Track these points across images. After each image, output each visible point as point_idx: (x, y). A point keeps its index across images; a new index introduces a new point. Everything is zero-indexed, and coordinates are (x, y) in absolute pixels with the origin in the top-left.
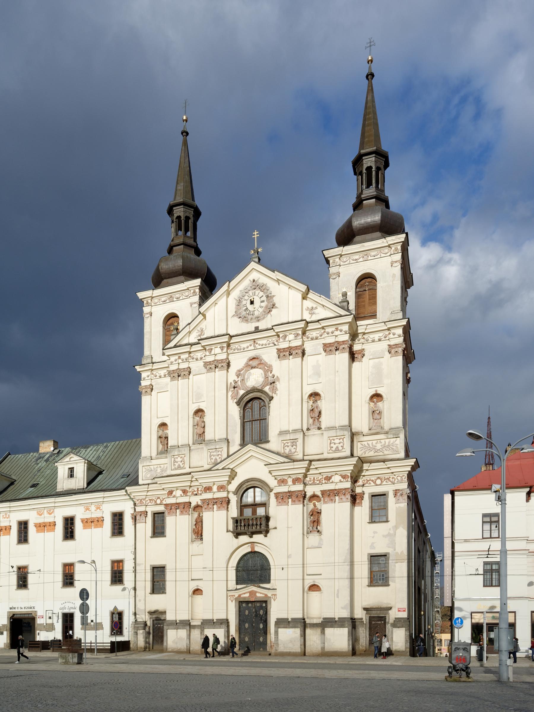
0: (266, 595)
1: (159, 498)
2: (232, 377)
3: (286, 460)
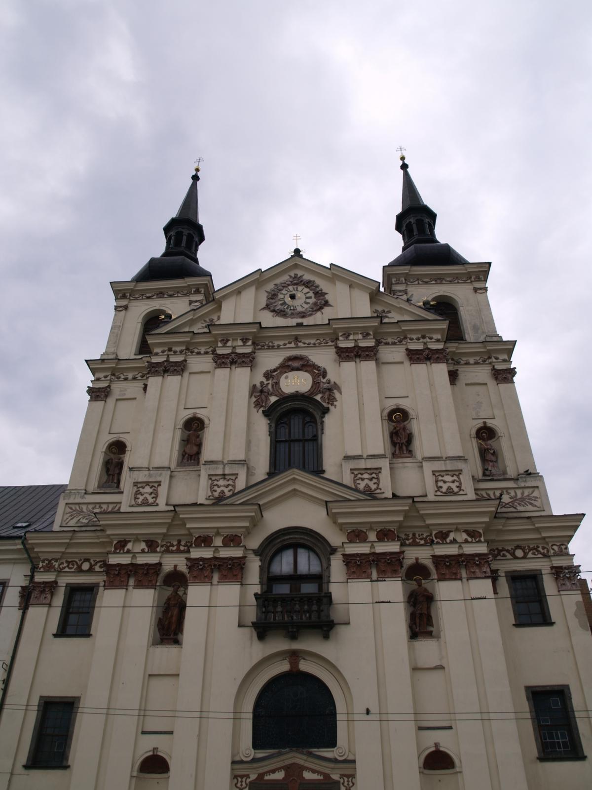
0: (327, 776)
1: (87, 560)
2: (259, 378)
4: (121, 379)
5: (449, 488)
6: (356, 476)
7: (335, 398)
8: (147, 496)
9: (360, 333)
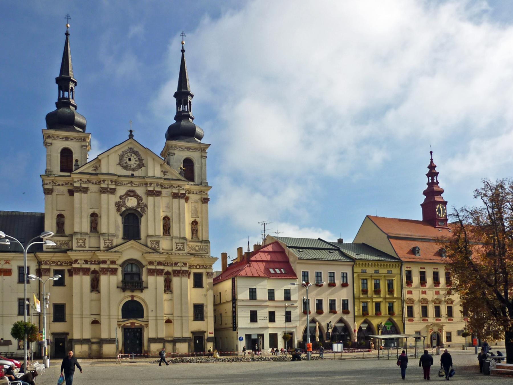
0: (141, 325)
1: (59, 261)
2: (114, 199)
3: (154, 251)
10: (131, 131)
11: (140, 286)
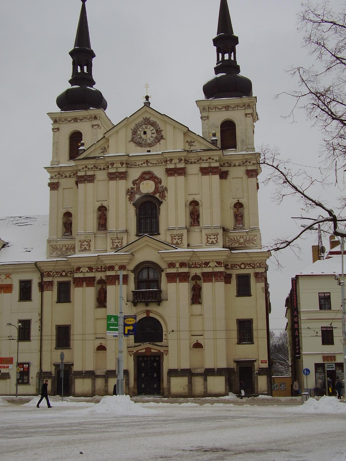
0: (159, 351)
1: (64, 271)
4: (63, 177)
5: (212, 241)
6: (172, 237)
7: (165, 196)
8: (85, 246)
9: (178, 159)
10: (147, 98)
11: (157, 298)
